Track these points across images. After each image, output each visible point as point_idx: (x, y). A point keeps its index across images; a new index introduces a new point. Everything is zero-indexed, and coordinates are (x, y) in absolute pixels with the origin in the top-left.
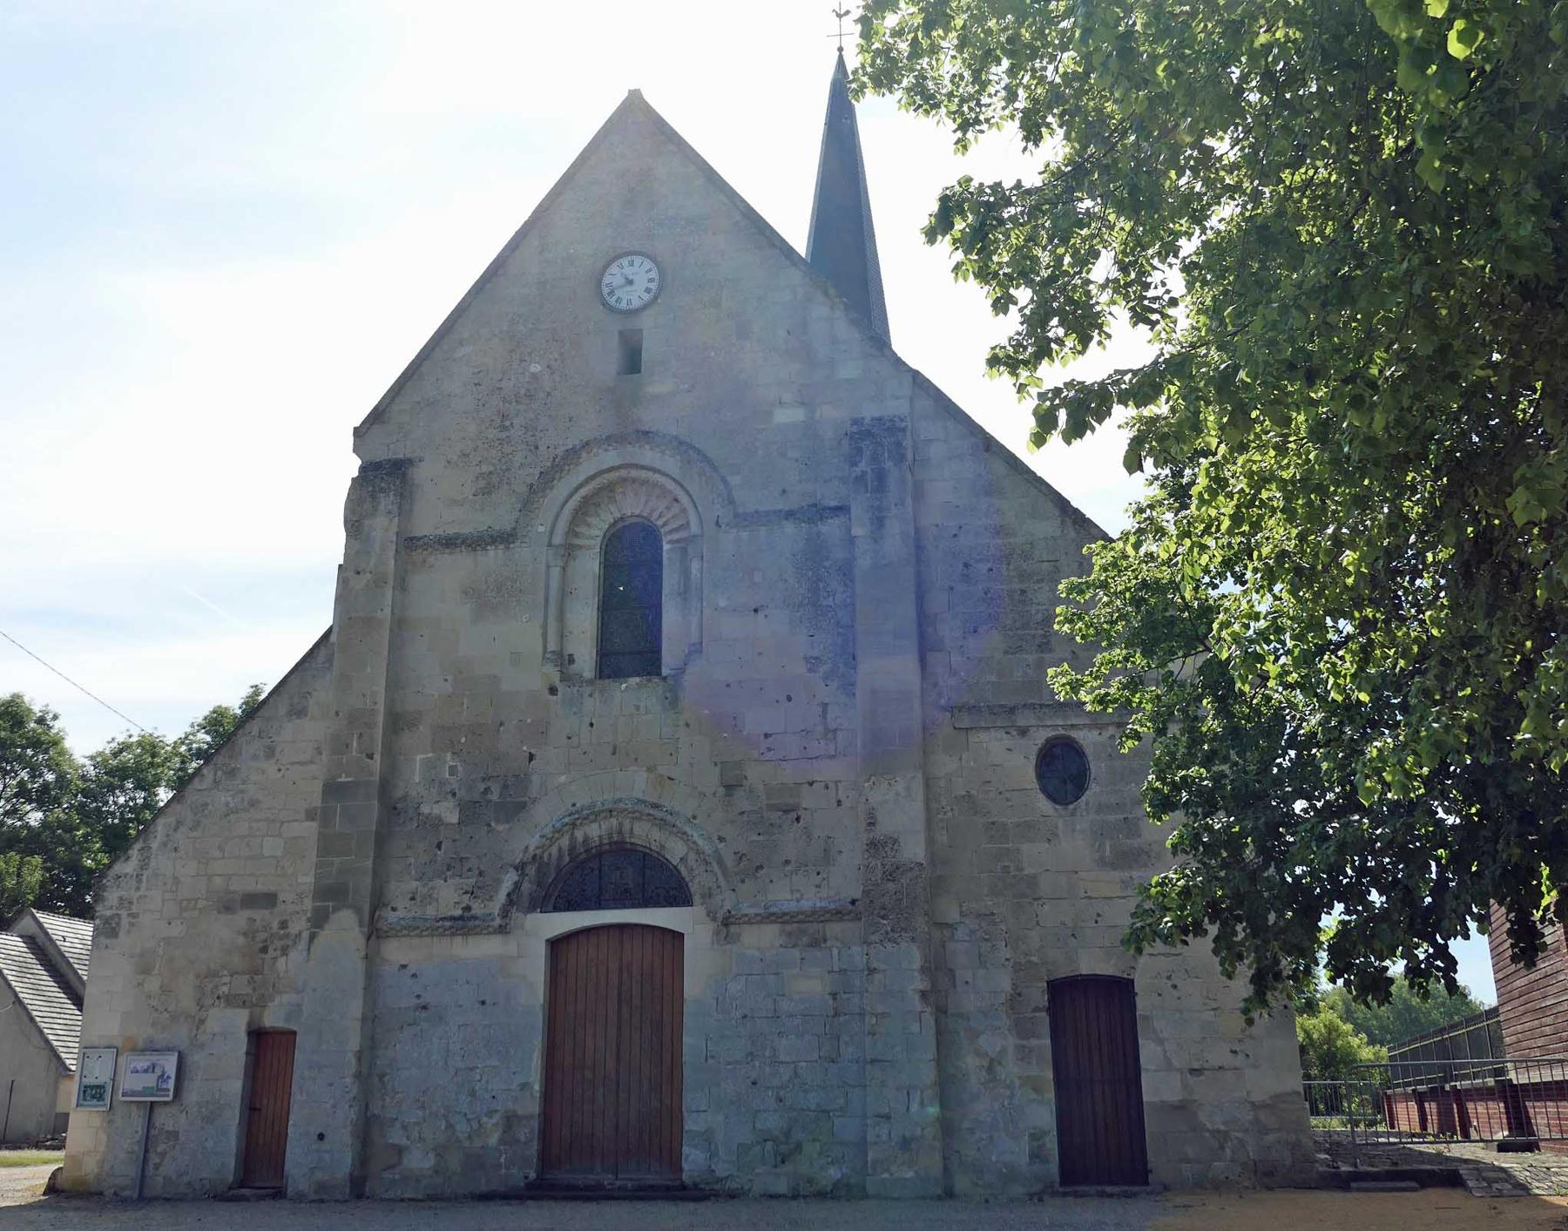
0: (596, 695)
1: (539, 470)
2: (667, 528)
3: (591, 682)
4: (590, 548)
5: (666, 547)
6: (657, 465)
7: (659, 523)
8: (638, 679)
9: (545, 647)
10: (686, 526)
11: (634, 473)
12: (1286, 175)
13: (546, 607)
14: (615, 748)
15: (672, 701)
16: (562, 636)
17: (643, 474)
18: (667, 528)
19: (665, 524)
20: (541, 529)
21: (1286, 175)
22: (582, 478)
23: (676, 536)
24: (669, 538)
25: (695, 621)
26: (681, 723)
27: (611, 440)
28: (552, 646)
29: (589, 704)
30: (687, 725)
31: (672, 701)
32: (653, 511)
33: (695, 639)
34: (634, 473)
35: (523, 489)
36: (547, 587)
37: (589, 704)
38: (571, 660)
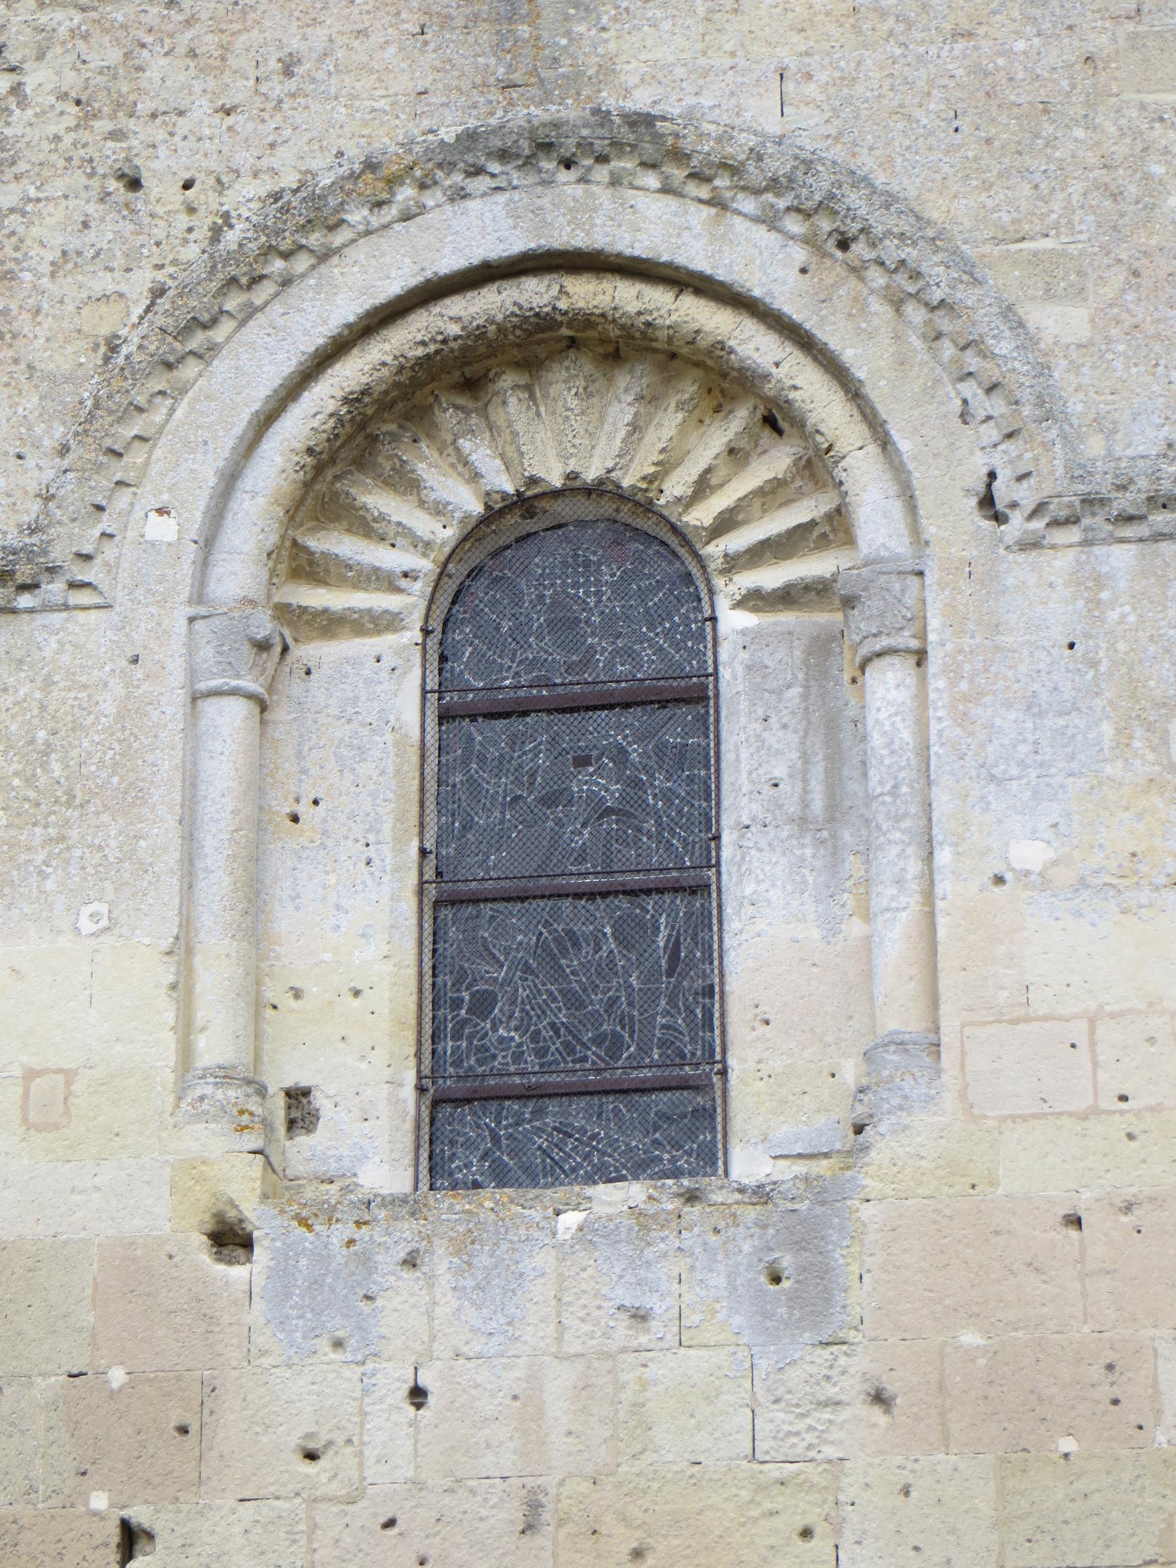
0: (441, 1262)
1: (143, 279)
2: (738, 541)
3: (406, 1206)
4: (385, 623)
5: (734, 621)
6: (695, 256)
7: (702, 515)
8: (636, 1191)
9: (186, 1053)
10: (836, 528)
11: (586, 293)
12: (532, 108)
13: (189, 886)
14: (534, 1507)
15: (797, 1276)
16: (259, 1007)
17: (627, 298)
18: (738, 541)
19: (725, 523)
20: (162, 529)
21: (532, 108)
22: (347, 309)
23: (771, 577)
24: (747, 580)
25: (896, 938)
26: (851, 1388)
27: (472, 158)
28: (216, 1046)
29: (403, 1305)
30: (879, 1398)
31: (797, 1276)
32: (665, 467)
33: (899, 1015)
34: (586, 293)
35: (74, 357)
36: (191, 781)
37: (403, 1305)
38: (300, 1107)
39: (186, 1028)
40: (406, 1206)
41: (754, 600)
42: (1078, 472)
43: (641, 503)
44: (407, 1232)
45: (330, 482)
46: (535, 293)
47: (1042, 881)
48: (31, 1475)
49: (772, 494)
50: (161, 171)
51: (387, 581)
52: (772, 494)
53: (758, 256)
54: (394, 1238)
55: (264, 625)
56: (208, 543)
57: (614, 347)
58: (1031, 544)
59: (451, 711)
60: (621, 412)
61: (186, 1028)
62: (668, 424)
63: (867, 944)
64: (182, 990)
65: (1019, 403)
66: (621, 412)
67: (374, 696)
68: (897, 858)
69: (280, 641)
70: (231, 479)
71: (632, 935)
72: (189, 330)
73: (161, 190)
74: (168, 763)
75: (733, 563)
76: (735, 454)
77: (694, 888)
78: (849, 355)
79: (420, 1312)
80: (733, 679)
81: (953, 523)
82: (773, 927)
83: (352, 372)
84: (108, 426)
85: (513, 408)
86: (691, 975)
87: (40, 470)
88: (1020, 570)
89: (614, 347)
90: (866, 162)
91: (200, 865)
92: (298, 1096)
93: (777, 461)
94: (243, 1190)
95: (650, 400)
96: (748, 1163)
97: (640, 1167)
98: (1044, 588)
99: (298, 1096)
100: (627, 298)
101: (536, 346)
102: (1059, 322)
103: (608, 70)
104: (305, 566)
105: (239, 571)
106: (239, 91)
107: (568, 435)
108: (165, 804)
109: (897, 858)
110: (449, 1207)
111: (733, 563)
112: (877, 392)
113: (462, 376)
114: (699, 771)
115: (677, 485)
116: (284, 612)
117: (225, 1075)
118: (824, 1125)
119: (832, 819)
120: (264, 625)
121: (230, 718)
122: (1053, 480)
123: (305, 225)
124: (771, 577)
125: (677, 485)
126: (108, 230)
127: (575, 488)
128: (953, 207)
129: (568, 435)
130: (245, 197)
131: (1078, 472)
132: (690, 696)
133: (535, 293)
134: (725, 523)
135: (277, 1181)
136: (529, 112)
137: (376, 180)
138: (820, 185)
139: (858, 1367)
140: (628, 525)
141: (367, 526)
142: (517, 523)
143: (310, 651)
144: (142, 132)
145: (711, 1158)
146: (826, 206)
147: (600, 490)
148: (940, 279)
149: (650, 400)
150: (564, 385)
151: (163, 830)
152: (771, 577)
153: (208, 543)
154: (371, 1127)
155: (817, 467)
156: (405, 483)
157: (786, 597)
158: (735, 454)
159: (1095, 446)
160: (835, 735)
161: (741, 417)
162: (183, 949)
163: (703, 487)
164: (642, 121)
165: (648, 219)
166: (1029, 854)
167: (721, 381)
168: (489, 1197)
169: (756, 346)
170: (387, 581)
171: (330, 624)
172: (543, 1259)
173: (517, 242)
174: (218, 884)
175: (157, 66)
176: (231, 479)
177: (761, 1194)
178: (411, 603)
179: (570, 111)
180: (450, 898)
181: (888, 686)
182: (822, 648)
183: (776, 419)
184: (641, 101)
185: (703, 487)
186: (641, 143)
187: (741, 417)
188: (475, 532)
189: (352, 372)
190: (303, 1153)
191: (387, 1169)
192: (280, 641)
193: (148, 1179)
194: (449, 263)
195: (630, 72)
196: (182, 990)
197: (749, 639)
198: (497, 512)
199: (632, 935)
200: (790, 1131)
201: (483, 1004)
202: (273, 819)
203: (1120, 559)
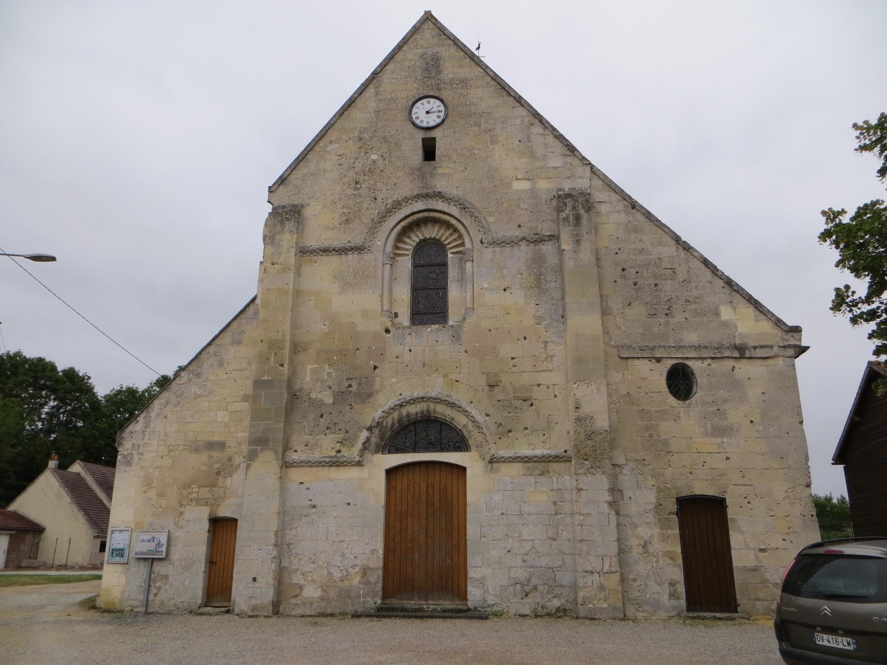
0: (413, 334)
1: (377, 211)
2: (451, 246)
3: (409, 327)
4: (407, 255)
5: (450, 256)
6: (446, 210)
7: (446, 242)
8: (437, 326)
10: (463, 244)
11: (432, 214)
16: (391, 302)
17: (437, 215)
18: (451, 246)
19: (449, 243)
20: (379, 243)
22: (403, 216)
26: (462, 350)
28: (386, 308)
29: (408, 339)
31: (456, 336)
33: (469, 305)
34: (432, 214)
36: (383, 275)
37: (408, 339)
38: (396, 315)
39: (382, 306)
40: (409, 327)
41: (453, 253)
42: (493, 238)
43: (439, 240)
44: (409, 330)
45: (400, 238)
46: (426, 214)
47: (487, 289)
48: (570, 487)
49: (455, 240)
50: (379, 197)
51: (407, 250)
52: (455, 240)
53: (454, 210)
54: (407, 331)
55: (392, 255)
56: (385, 245)
57: (435, 221)
58: (487, 247)
59: (415, 266)
60: (436, 229)
61: (382, 306)
62: (442, 231)
63: (466, 297)
64: (382, 301)
65: (486, 230)
66: (436, 229)
67: (406, 264)
68: (469, 286)
69: (394, 257)
70: (388, 237)
71: (437, 294)
72: (383, 218)
73: (379, 200)
74: (380, 272)
75: (450, 248)
76: (451, 235)
77: (445, 289)
78: (465, 223)
79: (411, 340)
80: (450, 263)
81: (477, 244)
82: (454, 292)
83: (403, 224)
84: (373, 230)
85: (423, 229)
86: (444, 299)
87: (364, 235)
88: (485, 250)
89: (435, 221)
90: (467, 199)
91: (347, 245)
92: (396, 314)
93: (455, 236)
94: (389, 325)
95: (440, 228)
96: (451, 323)
97: (437, 323)
98: (488, 253)
99: (396, 314)
100: (437, 215)
101: (426, 221)
102: (491, 219)
103: (435, 186)
104: (397, 248)
105: (389, 249)
106: (389, 187)
107: (430, 232)
108: (380, 277)
109: (469, 286)
110: (414, 328)
111: (450, 248)
112: (468, 228)
113: (416, 225)
114: (445, 274)
115: (443, 239)
116: (394, 254)
117: (387, 311)
118: (460, 318)
119: (462, 281)
120: (392, 255)
121: (388, 267)
122: (489, 239)
123: (398, 205)
124: (455, 250)
125: (443, 239)
126: (373, 205)
127: (430, 238)
128: (478, 205)
129: (430, 232)
130: (390, 201)
131: (493, 238)
132: (444, 265)
133: (426, 214)
134: (449, 243)
135: (393, 324)
136: (426, 191)
137: (406, 199)
138: (462, 201)
139: (463, 348)
140: (437, 245)
141: (405, 243)
142: (423, 243)
143: (399, 258)
144: (377, 193)
145: (446, 322)
146: (462, 204)
147: (434, 239)
148: (476, 214)
149: (440, 228)
150: (429, 226)
151: (380, 280)
152: (455, 250)
153: (385, 245)
154: (404, 318)
155: (460, 237)
156: (410, 238)
157: (456, 253)
158: (451, 235)
159: (495, 235)
160: (462, 270)
161: (451, 230)
162: (382, 296)
163: (447, 239)
164: (440, 193)
165: (440, 205)
166: (486, 286)
167: (449, 226)
168: (419, 326)
169: (453, 221)
170: (407, 250)
171: (400, 255)
172: (425, 334)
173: (424, 208)
174: (386, 287)
175: (379, 184)
176: (388, 237)
177: (452, 326)
178: (410, 253)
179: (430, 191)
180: (415, 290)
181: (469, 265)
182: (461, 259)
183: (456, 230)
184: (439, 190)
185: (447, 239)
186: (440, 195)
187: (451, 230)
188: (418, 244)
189: (403, 224)
190: (397, 320)
191: (406, 323)
192: (394, 257)
193: (376, 325)
194: (415, 210)
195: (438, 186)
196: (382, 301)
197: (452, 258)
198: (421, 241)
199: (437, 294)
200: (456, 319)
201: (418, 302)
202: (393, 279)
203: (497, 249)
